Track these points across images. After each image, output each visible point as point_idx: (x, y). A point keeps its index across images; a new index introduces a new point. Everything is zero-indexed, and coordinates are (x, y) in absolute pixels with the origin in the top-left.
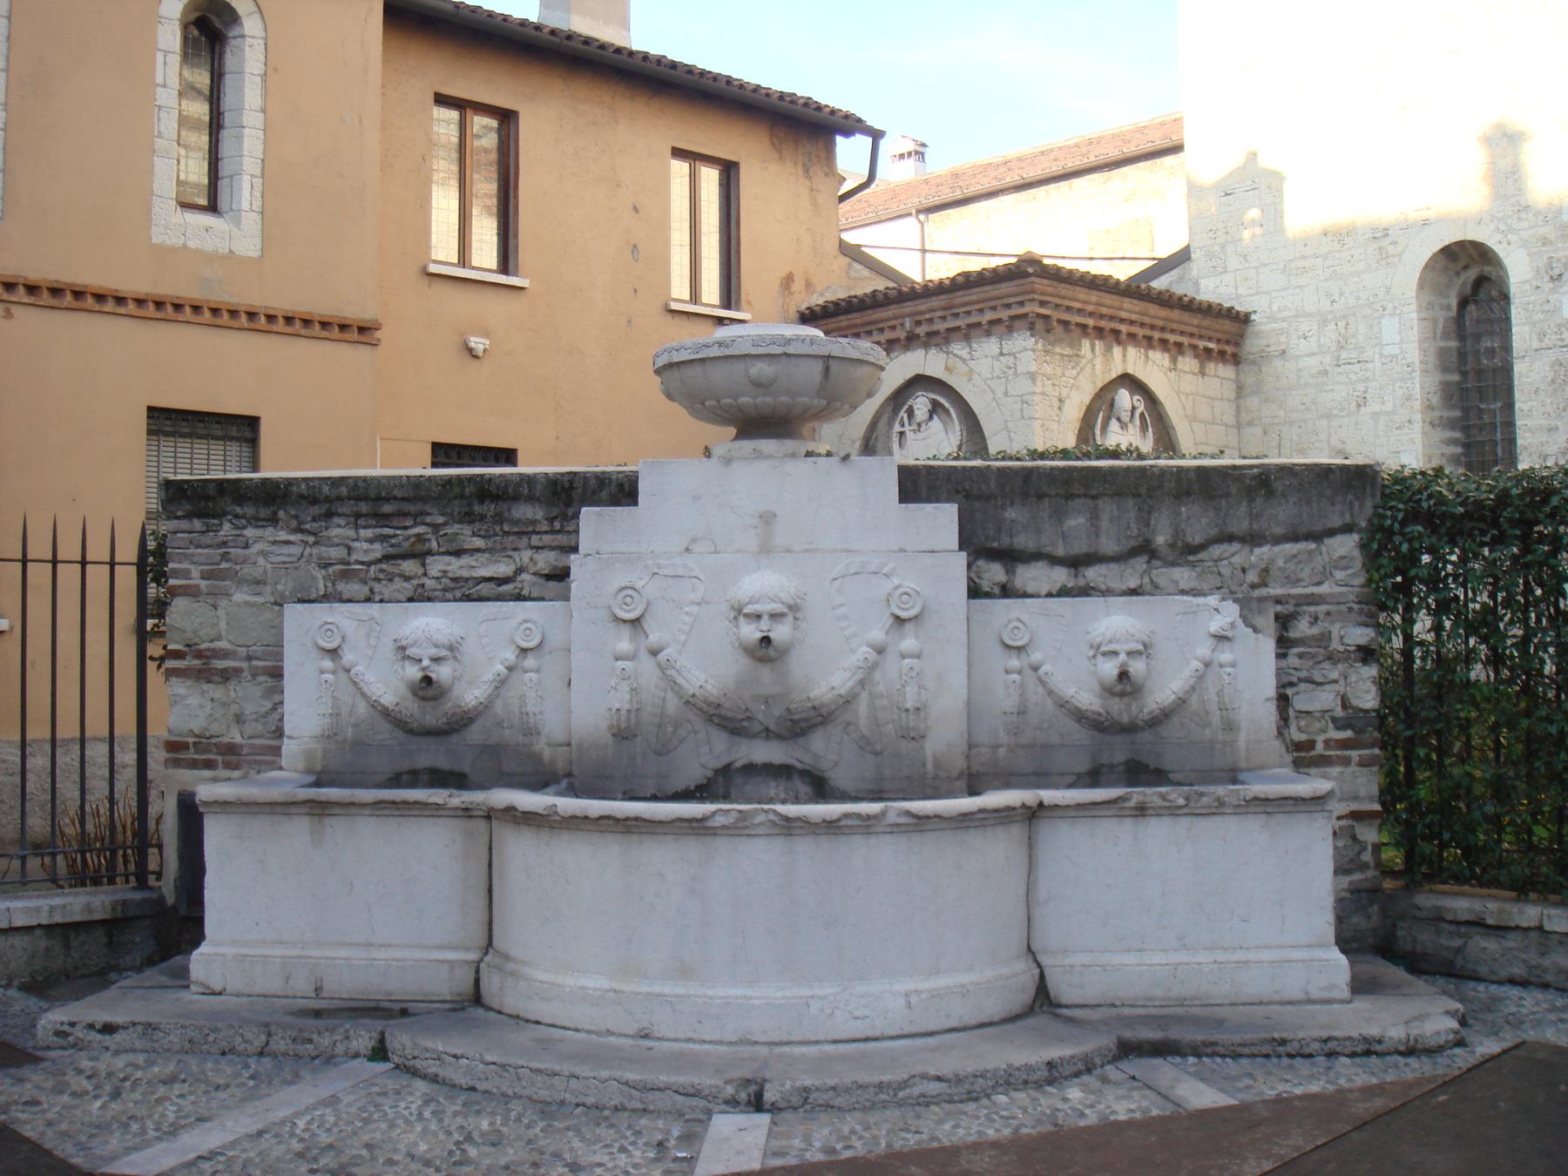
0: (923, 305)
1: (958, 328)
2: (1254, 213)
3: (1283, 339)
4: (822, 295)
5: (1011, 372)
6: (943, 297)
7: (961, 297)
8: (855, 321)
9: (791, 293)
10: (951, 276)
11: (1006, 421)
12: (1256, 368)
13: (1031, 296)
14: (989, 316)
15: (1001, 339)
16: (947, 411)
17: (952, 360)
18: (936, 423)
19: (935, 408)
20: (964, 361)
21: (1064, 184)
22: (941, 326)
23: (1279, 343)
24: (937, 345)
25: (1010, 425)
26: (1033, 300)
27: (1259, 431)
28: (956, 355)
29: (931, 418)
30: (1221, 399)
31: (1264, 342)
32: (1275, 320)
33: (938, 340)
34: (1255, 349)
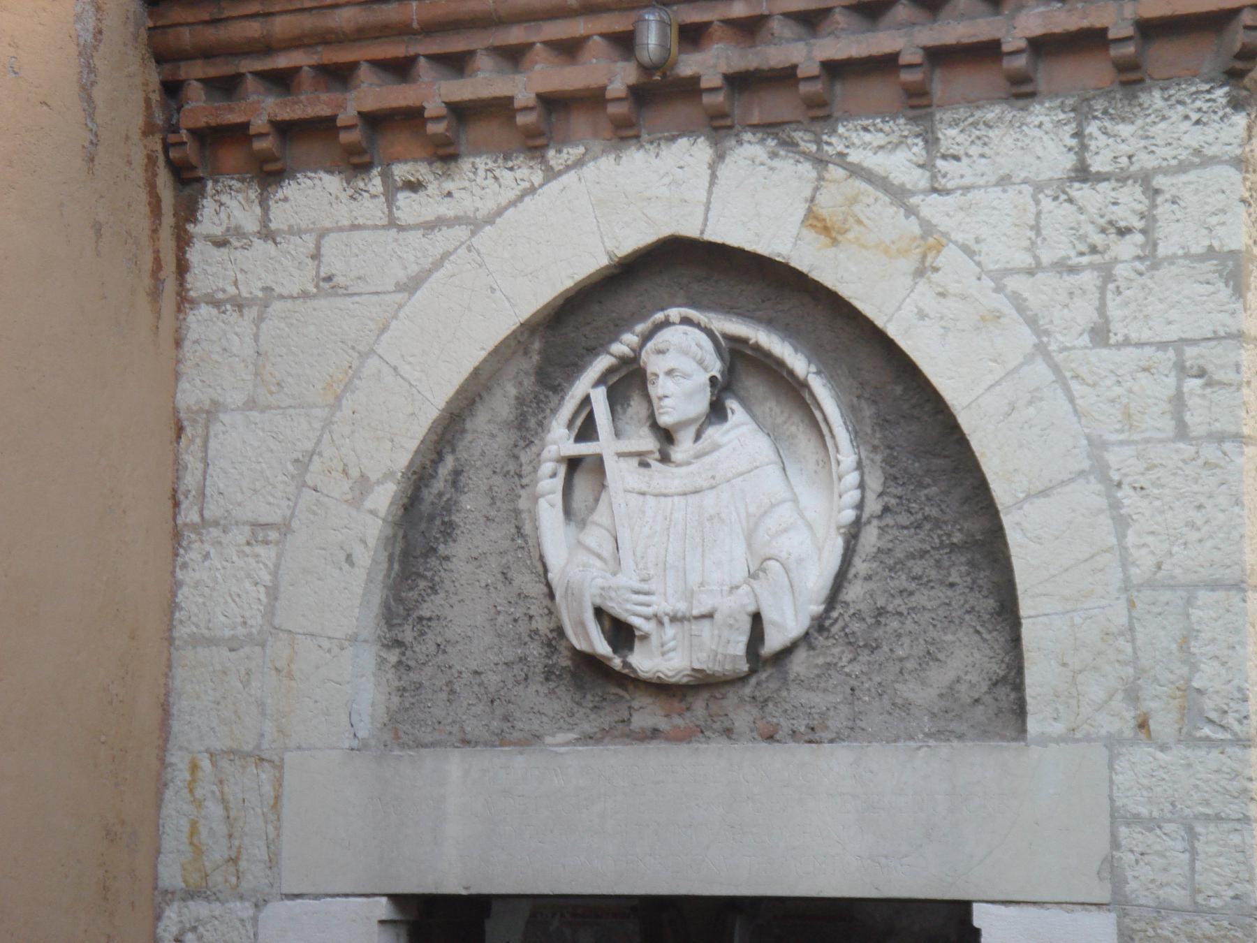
5: (1126, 248)
15: (1082, 112)
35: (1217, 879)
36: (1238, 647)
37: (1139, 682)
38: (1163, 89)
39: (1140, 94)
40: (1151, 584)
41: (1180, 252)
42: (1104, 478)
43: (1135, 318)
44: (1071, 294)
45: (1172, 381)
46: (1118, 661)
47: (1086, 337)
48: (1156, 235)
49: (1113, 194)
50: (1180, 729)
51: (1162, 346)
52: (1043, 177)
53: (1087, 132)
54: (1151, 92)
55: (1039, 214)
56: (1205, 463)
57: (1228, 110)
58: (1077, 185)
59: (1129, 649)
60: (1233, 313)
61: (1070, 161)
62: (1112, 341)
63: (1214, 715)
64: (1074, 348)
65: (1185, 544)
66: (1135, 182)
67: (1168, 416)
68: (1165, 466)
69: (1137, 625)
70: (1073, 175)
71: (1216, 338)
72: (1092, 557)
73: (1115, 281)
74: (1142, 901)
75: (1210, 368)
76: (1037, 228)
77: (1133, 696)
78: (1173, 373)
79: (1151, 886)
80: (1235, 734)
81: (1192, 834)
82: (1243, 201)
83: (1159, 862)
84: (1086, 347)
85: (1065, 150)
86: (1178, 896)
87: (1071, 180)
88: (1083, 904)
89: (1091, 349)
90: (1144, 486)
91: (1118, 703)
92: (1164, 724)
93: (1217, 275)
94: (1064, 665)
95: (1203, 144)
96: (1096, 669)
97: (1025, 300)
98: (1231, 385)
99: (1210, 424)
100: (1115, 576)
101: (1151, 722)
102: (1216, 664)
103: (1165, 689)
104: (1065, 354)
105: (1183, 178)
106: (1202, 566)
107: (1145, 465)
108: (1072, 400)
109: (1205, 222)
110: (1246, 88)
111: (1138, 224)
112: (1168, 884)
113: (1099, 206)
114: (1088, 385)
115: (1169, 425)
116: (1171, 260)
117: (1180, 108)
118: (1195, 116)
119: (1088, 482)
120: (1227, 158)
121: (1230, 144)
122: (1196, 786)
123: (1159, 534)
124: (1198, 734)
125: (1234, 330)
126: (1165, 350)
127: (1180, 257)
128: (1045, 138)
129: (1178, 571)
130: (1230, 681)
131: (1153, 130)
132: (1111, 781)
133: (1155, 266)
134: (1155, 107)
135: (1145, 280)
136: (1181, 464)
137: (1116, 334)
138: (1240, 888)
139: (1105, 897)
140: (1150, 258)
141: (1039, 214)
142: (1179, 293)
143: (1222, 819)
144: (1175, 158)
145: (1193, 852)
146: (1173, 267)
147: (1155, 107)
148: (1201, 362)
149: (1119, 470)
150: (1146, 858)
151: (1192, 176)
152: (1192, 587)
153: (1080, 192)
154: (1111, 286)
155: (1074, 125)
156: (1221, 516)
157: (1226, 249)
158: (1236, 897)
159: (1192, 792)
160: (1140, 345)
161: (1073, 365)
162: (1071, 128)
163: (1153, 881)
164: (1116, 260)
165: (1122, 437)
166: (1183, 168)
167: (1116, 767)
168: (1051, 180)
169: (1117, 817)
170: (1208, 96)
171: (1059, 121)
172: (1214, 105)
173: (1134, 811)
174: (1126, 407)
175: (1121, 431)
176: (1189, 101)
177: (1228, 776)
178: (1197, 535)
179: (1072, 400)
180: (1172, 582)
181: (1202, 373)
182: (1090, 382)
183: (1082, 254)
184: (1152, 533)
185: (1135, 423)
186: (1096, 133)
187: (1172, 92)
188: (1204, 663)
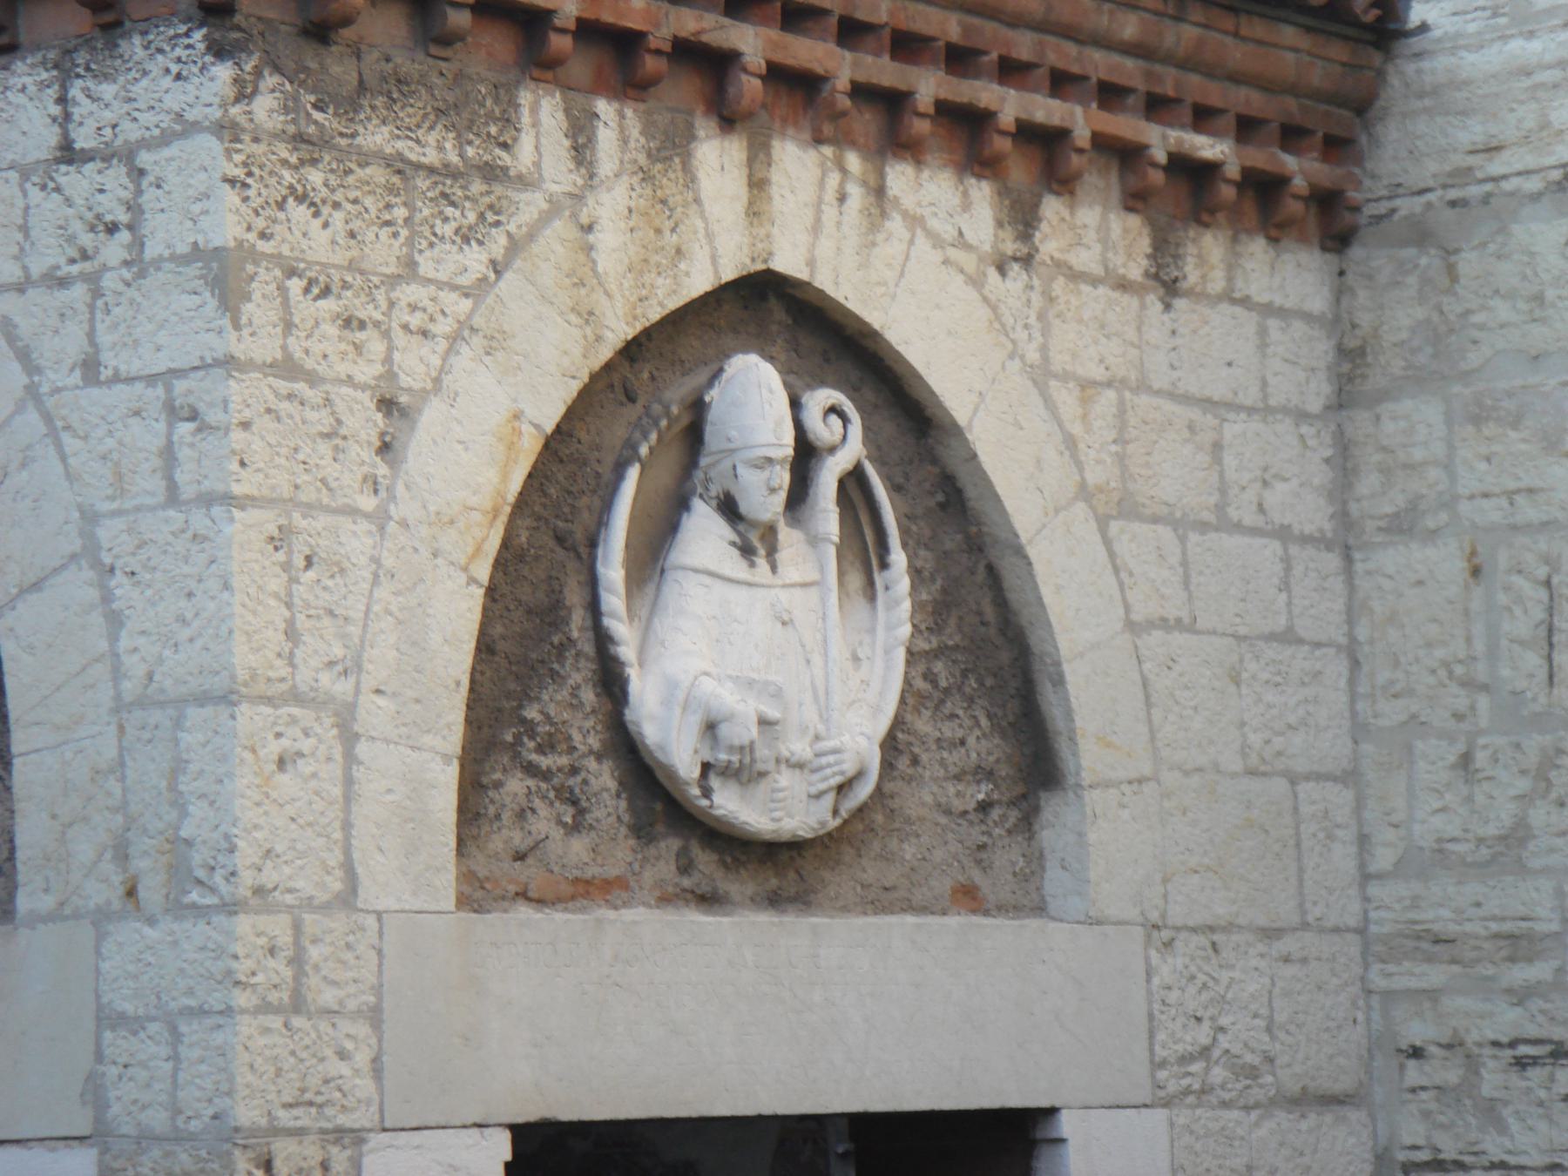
5: (114, 250)
12: (1429, 260)
15: (65, 72)
25: (103, 534)
27: (1446, 560)
31: (1474, 132)
35: (198, 1094)
36: (226, 781)
37: (129, 834)
38: (144, 33)
39: (120, 42)
40: (141, 703)
41: (166, 253)
42: (96, 564)
43: (125, 344)
44: (62, 315)
45: (161, 427)
46: (107, 808)
47: (78, 373)
48: (143, 232)
49: (99, 178)
50: (167, 896)
51: (151, 379)
52: (31, 158)
53: (70, 95)
54: (131, 37)
55: (27, 208)
56: (195, 536)
57: (208, 59)
58: (63, 168)
59: (118, 792)
60: (220, 332)
61: (52, 136)
62: (102, 378)
63: (201, 873)
64: (64, 388)
65: (176, 645)
66: (120, 161)
67: (159, 475)
68: (155, 542)
69: (127, 758)
70: (58, 154)
71: (203, 367)
72: (84, 669)
73: (103, 295)
74: (125, 1130)
75: (201, 407)
76: (25, 229)
77: (122, 854)
78: (163, 416)
79: (133, 1108)
80: (222, 898)
81: (176, 1036)
82: (232, 182)
83: (143, 1075)
84: (77, 387)
85: (49, 121)
86: (157, 1119)
87: (58, 161)
88: (66, 1138)
89: (82, 388)
90: (137, 571)
91: (107, 867)
92: (152, 892)
93: (202, 281)
94: (54, 817)
95: (184, 106)
96: (86, 819)
97: (16, 326)
98: (218, 428)
99: (199, 482)
100: (105, 694)
101: (140, 887)
102: (205, 804)
103: (154, 841)
104: (56, 396)
105: (166, 152)
106: (191, 674)
107: (136, 542)
108: (63, 458)
109: (188, 211)
110: (239, 28)
111: (123, 217)
112: (150, 1105)
113: (85, 195)
114: (80, 438)
115: (158, 485)
116: (157, 263)
117: (160, 57)
118: (174, 68)
119: (80, 569)
120: (207, 123)
121: (210, 105)
122: (182, 970)
123: (150, 634)
124: (187, 900)
125: (219, 354)
126: (154, 386)
127: (166, 260)
128: (29, 105)
129: (168, 683)
130: (217, 826)
131: (137, 89)
132: (98, 971)
133: (142, 274)
134: (136, 58)
135: (132, 293)
136: (170, 538)
137: (106, 367)
138: (221, 1103)
139: (82, 1127)
140: (137, 264)
141: (27, 208)
142: (167, 308)
143: (206, 1012)
144: (157, 126)
145: (175, 1058)
146: (160, 274)
147: (136, 58)
148: (191, 400)
149: (110, 550)
150: (130, 1070)
151: (172, 150)
152: (182, 702)
153: (67, 176)
154: (100, 303)
155: (56, 87)
156: (212, 606)
157: (211, 246)
158: (215, 1117)
159: (178, 980)
160: (130, 380)
161: (64, 412)
162: (52, 92)
163: (135, 1102)
164: (105, 268)
165: (114, 506)
166: (166, 139)
167: (103, 950)
168: (38, 162)
169: (108, 1019)
170: (187, 41)
171: (42, 82)
172: (193, 52)
173: (120, 1009)
174: (117, 464)
175: (112, 498)
176: (168, 49)
177: (213, 954)
178: (186, 633)
179: (63, 458)
180: (162, 698)
181: (194, 416)
182: (82, 434)
183: (72, 261)
184: (143, 632)
185: (126, 486)
186: (80, 97)
187: (151, 37)
188: (193, 804)
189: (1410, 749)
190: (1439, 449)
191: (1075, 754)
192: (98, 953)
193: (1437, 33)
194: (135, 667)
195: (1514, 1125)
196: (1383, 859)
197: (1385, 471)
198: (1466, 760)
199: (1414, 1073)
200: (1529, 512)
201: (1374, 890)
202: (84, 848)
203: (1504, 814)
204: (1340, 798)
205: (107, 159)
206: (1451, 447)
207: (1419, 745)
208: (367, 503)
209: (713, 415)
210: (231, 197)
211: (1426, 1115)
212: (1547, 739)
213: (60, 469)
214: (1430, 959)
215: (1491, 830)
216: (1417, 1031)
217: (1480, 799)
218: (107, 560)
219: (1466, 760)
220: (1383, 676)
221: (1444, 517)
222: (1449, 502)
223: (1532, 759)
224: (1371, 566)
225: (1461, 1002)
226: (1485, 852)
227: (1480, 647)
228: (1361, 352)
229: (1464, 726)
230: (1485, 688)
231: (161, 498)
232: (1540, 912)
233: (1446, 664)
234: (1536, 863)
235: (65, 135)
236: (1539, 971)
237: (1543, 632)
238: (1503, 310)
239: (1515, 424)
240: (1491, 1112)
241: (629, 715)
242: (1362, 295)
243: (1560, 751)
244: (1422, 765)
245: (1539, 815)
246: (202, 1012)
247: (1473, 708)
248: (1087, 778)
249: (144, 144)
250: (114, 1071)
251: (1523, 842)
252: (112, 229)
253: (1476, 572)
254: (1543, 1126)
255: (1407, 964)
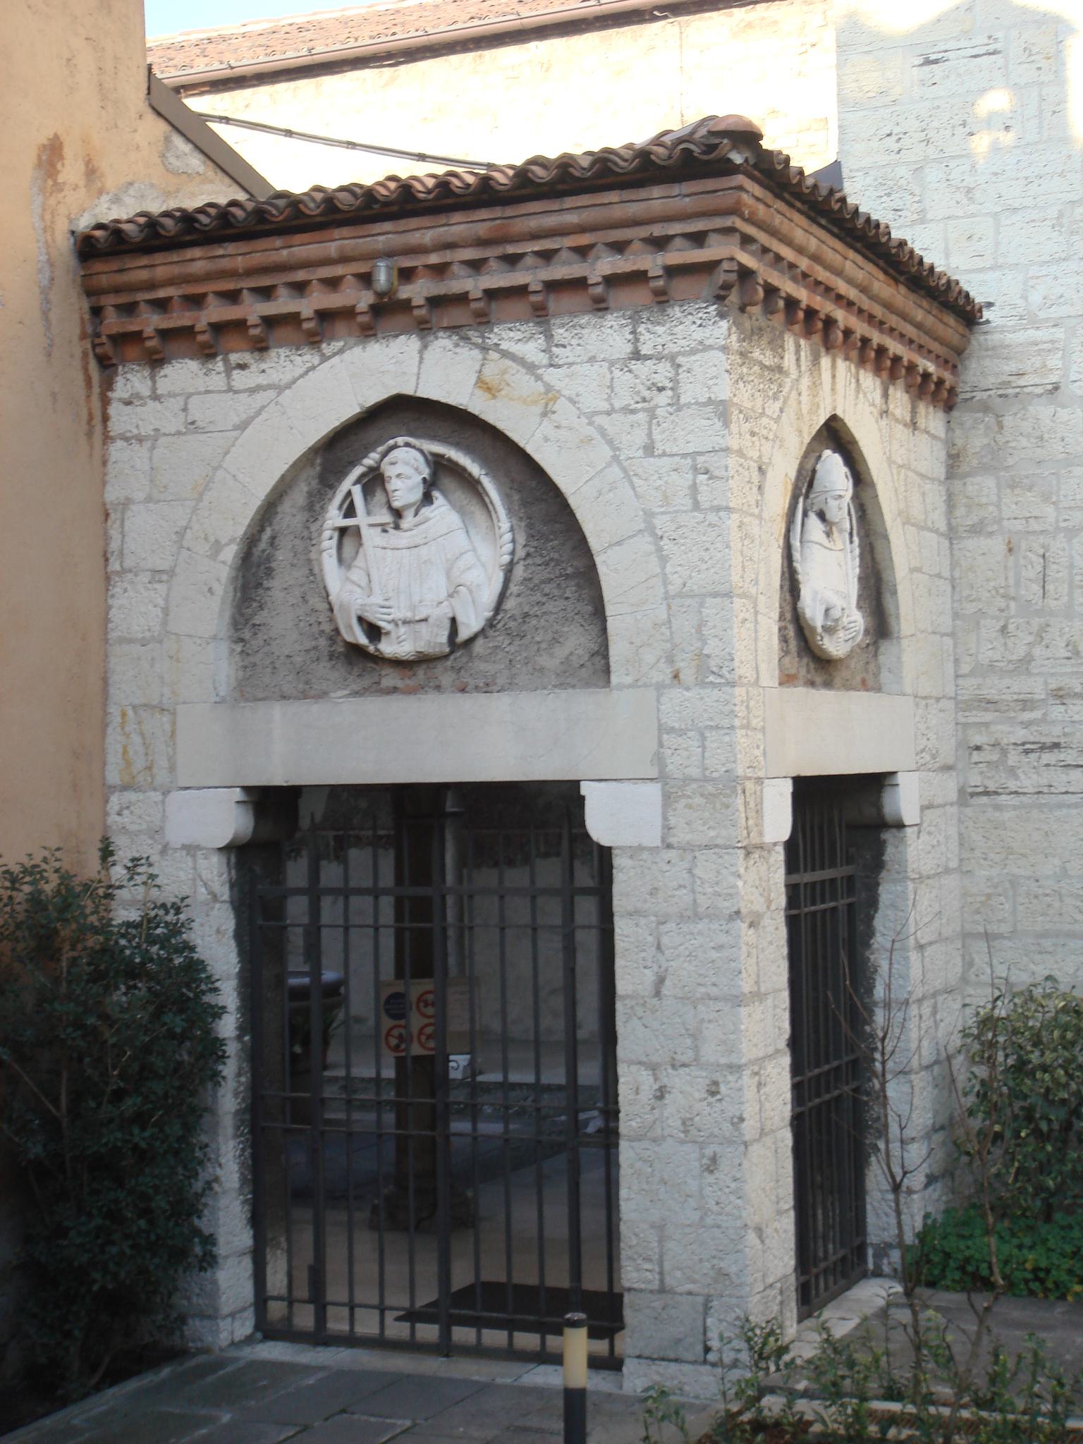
0: (425, 232)
1: (521, 291)
2: (997, 101)
3: (1054, 361)
4: (117, 200)
5: (663, 399)
6: (484, 214)
7: (537, 216)
8: (225, 264)
9: (58, 187)
10: (519, 161)
11: (649, 515)
12: (991, 419)
13: (728, 222)
14: (607, 264)
15: (635, 319)
16: (473, 486)
17: (493, 368)
18: (442, 512)
19: (441, 470)
20: (531, 368)
21: (305, 85)
22: (474, 285)
23: (1044, 369)
24: (453, 329)
25: (658, 522)
26: (730, 230)
27: (997, 545)
28: (506, 354)
29: (427, 499)
30: (932, 480)
31: (1012, 367)
32: (1035, 323)
33: (640, 295)
34: (990, 381)
40: (680, 595)
42: (653, 534)
45: (690, 476)
51: (684, 456)
61: (629, 348)
63: (715, 669)
75: (712, 469)
76: (611, 387)
77: (670, 660)
81: (703, 738)
83: (685, 753)
86: (695, 772)
87: (631, 359)
91: (662, 665)
92: (688, 675)
100: (660, 591)
105: (693, 358)
108: (634, 488)
115: (689, 502)
116: (688, 405)
118: (699, 322)
125: (723, 446)
129: (695, 587)
131: (676, 330)
132: (659, 710)
133: (679, 410)
138: (729, 766)
139: (654, 773)
153: (636, 366)
156: (719, 555)
162: (629, 329)
164: (657, 406)
166: (693, 352)
169: (662, 729)
179: (634, 488)
189: (978, 623)
190: (994, 498)
191: (899, 624)
192: (658, 701)
193: (993, 324)
194: (676, 581)
195: (1022, 776)
196: (965, 669)
197: (968, 506)
198: (1004, 629)
199: (976, 756)
200: (1035, 526)
201: (960, 681)
202: (649, 657)
203: (1021, 651)
204: (948, 641)
205: (660, 359)
206: (1000, 498)
207: (983, 622)
208: (756, 511)
209: (818, 476)
210: (727, 375)
211: (981, 773)
212: (1042, 620)
213: (631, 492)
214: (986, 710)
215: (1015, 657)
216: (978, 739)
217: (1010, 644)
218: (660, 533)
219: (1004, 629)
220: (965, 593)
221: (995, 527)
222: (999, 521)
223: (1035, 628)
224: (961, 546)
225: (999, 727)
226: (1011, 667)
227: (1011, 582)
228: (958, 456)
229: (1004, 614)
230: (1013, 598)
231: (690, 507)
232: (1036, 691)
233: (995, 588)
234: (1036, 671)
235: (636, 348)
236: (1036, 714)
237: (1041, 576)
238: (1024, 442)
239: (1030, 489)
240: (1012, 772)
241: (800, 605)
242: (958, 432)
243: (1048, 625)
244: (983, 630)
245: (1038, 651)
246: (717, 727)
247: (1008, 606)
248: (903, 634)
249: (679, 353)
250: (669, 752)
251: (1029, 662)
252: (661, 389)
253: (1010, 550)
254: (1035, 776)
255: (974, 712)
